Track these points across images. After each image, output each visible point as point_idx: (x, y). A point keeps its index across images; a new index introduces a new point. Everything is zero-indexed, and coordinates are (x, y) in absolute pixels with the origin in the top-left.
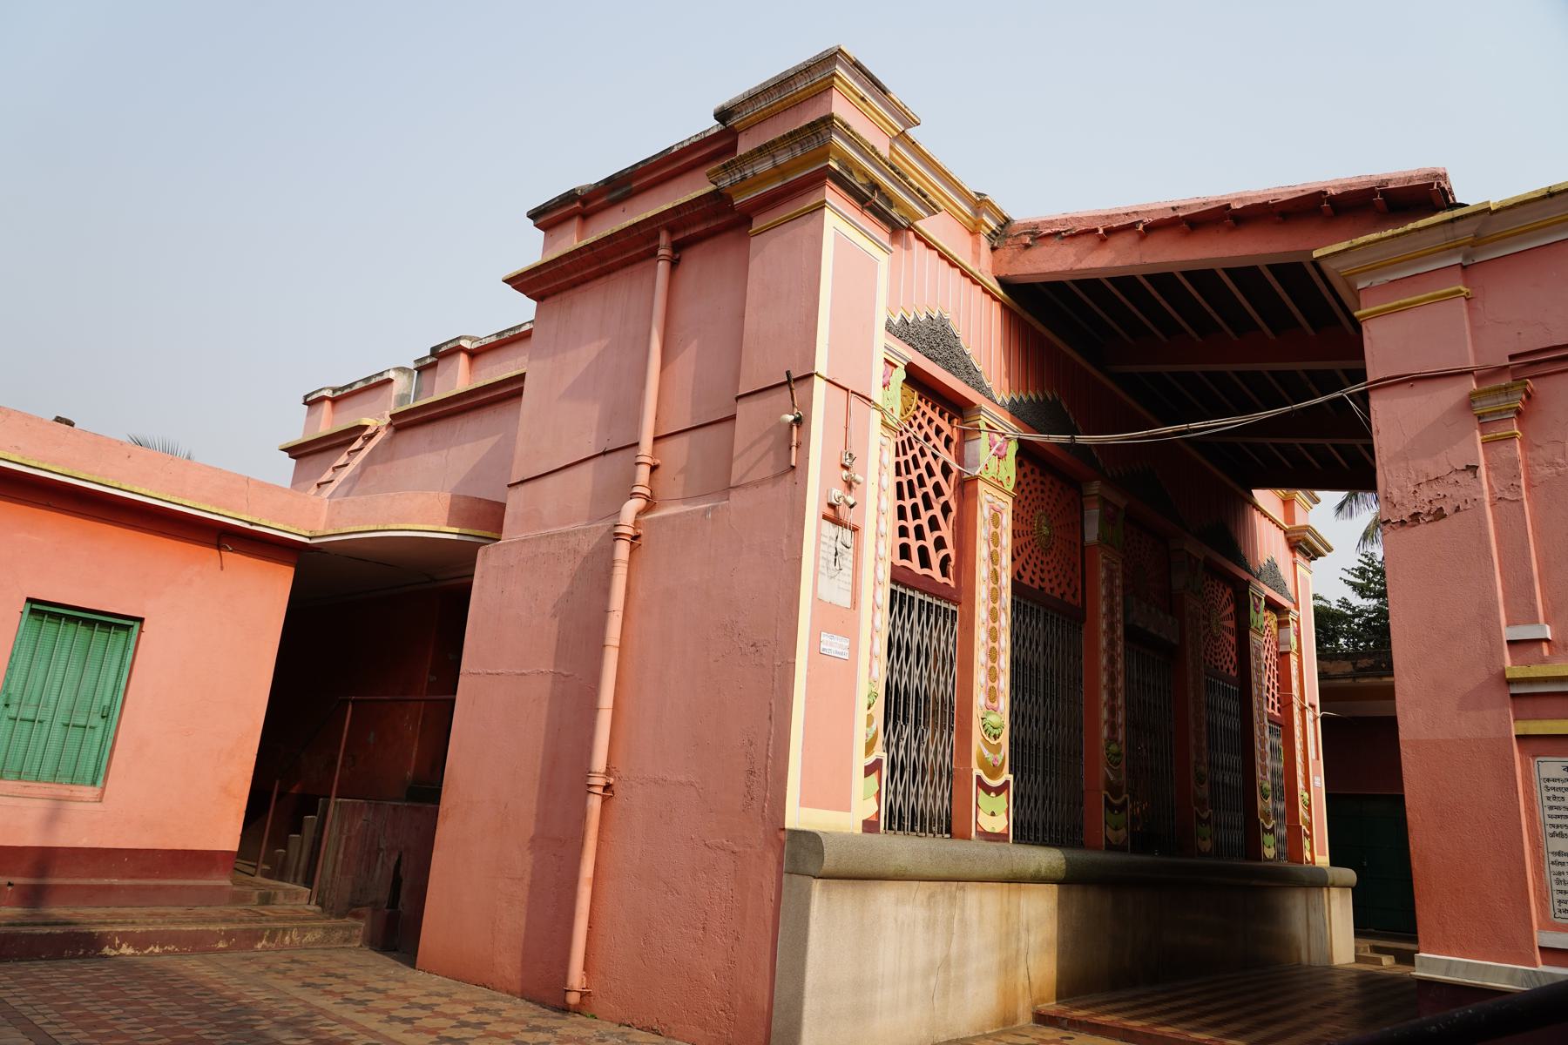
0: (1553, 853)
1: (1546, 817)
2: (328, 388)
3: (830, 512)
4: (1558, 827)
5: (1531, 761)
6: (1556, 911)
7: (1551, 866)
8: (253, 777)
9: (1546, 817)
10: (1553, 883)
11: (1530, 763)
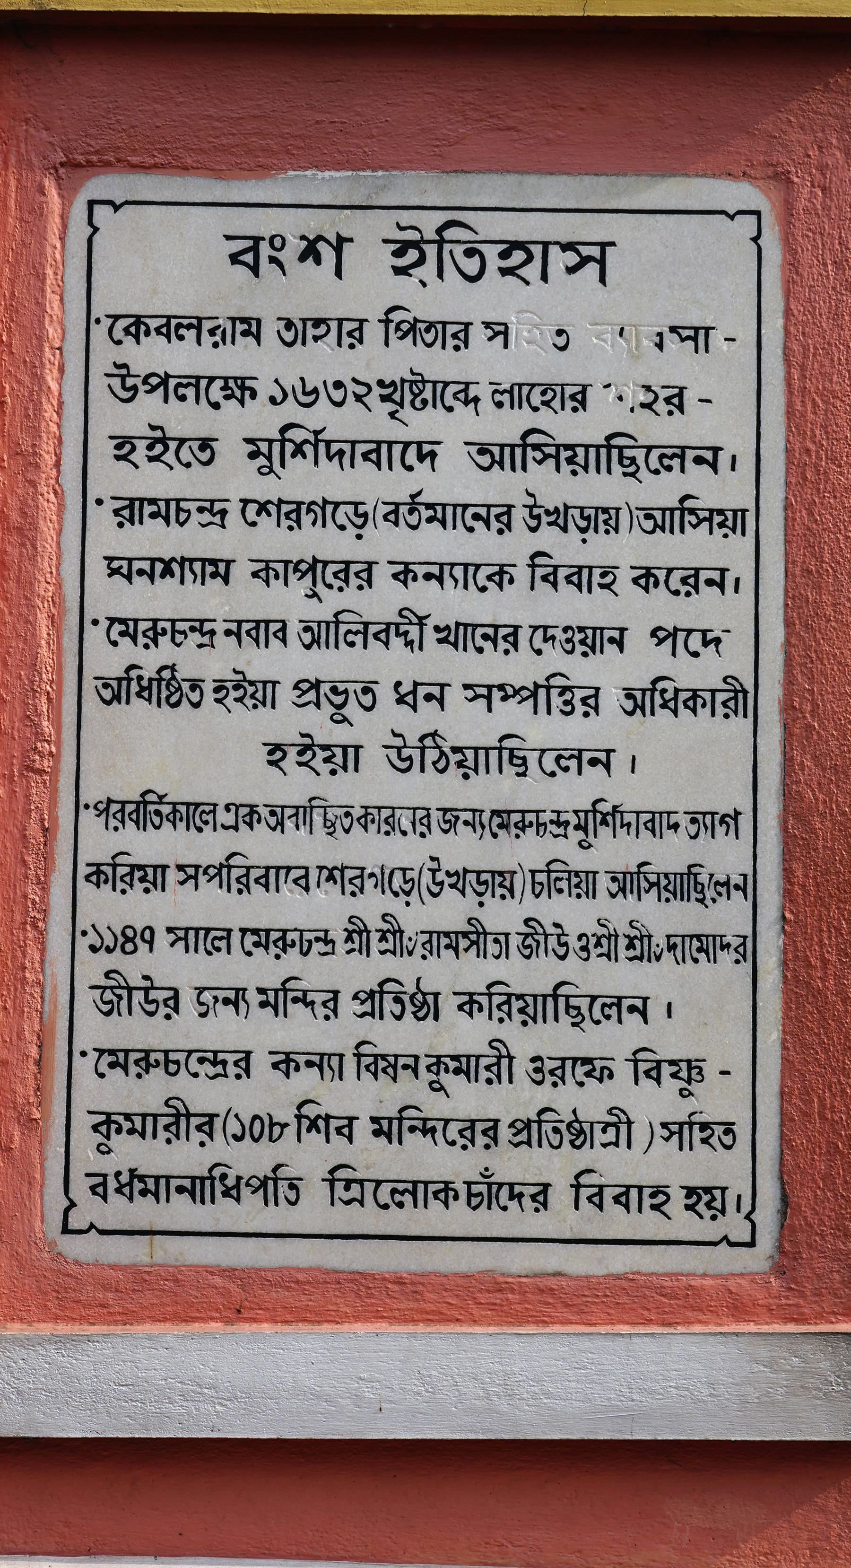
0: (104, 809)
1: (96, 568)
2: (201, 700)
3: (470, 694)
4: (155, 634)
5: (53, 193)
6: (80, 1188)
7: (85, 889)
8: (28, 1438)
9: (96, 568)
10: (85, 999)
11: (39, 213)
